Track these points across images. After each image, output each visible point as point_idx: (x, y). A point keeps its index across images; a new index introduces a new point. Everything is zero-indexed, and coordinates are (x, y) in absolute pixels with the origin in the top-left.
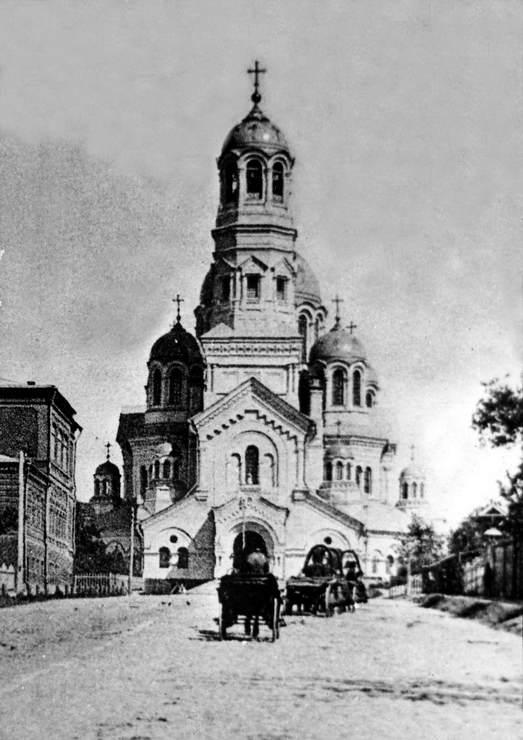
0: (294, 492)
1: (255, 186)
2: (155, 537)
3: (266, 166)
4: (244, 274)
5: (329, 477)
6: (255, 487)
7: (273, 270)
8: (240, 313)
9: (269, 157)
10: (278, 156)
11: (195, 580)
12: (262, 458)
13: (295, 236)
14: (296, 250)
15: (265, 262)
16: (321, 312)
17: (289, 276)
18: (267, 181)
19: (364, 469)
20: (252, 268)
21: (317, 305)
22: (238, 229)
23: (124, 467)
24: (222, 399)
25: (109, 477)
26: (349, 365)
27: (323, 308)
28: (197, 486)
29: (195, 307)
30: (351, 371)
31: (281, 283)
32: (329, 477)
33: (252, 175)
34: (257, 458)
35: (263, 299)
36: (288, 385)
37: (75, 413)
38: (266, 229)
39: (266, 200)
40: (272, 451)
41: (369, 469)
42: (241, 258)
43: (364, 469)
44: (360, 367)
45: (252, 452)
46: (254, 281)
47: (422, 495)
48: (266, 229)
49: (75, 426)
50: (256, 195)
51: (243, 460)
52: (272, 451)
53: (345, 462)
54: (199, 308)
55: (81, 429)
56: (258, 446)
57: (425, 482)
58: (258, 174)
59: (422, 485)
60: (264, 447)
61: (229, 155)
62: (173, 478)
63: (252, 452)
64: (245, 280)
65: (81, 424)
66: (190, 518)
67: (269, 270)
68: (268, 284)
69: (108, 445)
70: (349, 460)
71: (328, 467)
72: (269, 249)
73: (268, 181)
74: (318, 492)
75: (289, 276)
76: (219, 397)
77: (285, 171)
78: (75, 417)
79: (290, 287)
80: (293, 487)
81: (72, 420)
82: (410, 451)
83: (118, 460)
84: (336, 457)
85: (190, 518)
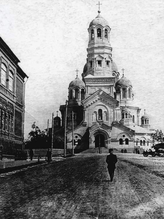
0: (113, 122)
1: (99, 35)
2: (70, 137)
3: (103, 29)
4: (97, 60)
5: (123, 117)
6: (102, 120)
7: (105, 59)
8: (96, 71)
9: (103, 27)
10: (106, 27)
11: (91, 38)
12: (103, 113)
13: (112, 50)
14: (112, 53)
15: (103, 56)
16: (118, 74)
17: (110, 61)
18: (103, 33)
19: (132, 116)
20: (98, 59)
21: (117, 72)
22: (105, 47)
23: (62, 117)
24: (90, 96)
25: (58, 121)
26: (127, 87)
27: (118, 73)
28: (84, 121)
29: (82, 74)
30: (128, 89)
31: (108, 62)
32: (123, 117)
33: (99, 32)
34: (102, 113)
35: (103, 67)
36: (110, 91)
37: (20, 62)
38: (103, 47)
39: (103, 39)
40: (106, 110)
41: (133, 116)
42: (96, 56)
43: (132, 116)
44: (130, 88)
45: (100, 111)
46: (100, 62)
47: (148, 123)
48: (103, 47)
49: (22, 74)
50: (100, 38)
51: (97, 113)
52: (106, 110)
53: (128, 113)
54: (82, 74)
55: (28, 77)
56: (100, 108)
57: (149, 120)
58: (100, 32)
59: (148, 120)
60: (104, 110)
61: (91, 27)
62: (76, 119)
63: (100, 111)
64: (97, 62)
65: (28, 76)
66: (80, 131)
67: (104, 59)
68: (104, 63)
69: (57, 112)
70: (129, 113)
71: (123, 115)
72: (104, 53)
73: (103, 34)
74: (119, 122)
75: (110, 61)
76: (90, 95)
77: (108, 31)
78: (19, 64)
79: (110, 64)
80: (112, 121)
81: (18, 66)
82: (144, 111)
83: (60, 116)
84: (126, 112)
85: (80, 131)
